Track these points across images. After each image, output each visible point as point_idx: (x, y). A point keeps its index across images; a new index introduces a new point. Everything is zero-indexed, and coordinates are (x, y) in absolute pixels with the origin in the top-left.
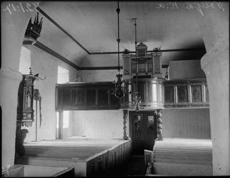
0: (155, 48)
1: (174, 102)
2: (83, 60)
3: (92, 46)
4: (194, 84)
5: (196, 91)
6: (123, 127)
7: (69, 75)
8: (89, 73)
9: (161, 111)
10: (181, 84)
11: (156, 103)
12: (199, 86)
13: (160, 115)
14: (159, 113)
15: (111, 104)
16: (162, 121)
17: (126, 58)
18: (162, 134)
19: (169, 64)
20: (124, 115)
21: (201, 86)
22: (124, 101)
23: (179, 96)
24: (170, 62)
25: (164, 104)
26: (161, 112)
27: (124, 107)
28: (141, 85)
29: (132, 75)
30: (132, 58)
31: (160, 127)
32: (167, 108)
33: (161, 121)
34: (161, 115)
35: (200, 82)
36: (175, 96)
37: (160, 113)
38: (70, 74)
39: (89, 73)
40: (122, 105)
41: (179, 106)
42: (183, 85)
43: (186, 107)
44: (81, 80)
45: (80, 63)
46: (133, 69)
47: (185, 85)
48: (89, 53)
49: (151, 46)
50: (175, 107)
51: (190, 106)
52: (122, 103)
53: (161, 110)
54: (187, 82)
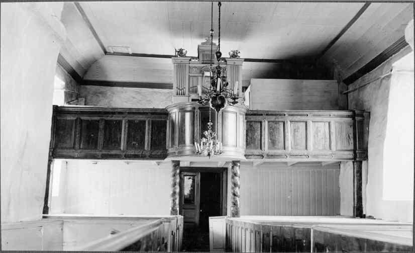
0: (232, 51)
1: (261, 149)
2: (90, 64)
3: (116, 43)
4: (273, 118)
5: (297, 131)
6: (172, 192)
7: (65, 92)
8: (101, 93)
9: (239, 164)
10: (274, 117)
11: (233, 149)
12: (258, 122)
13: (236, 171)
14: (235, 167)
15: (149, 149)
16: (240, 182)
17: (180, 67)
18: (239, 206)
19: (250, 84)
20: (173, 171)
21: (261, 123)
22: (177, 142)
23: (271, 139)
24: (253, 81)
25: (245, 151)
26: (239, 166)
27: (177, 154)
28: (206, 118)
29: (189, 96)
30: (191, 65)
31: (237, 193)
32: (250, 158)
33: (239, 183)
34: (239, 172)
35: (280, 115)
36: (264, 139)
37: (238, 168)
38: (68, 90)
39: (101, 93)
40: (170, 150)
41: (269, 156)
42: (277, 120)
43: (274, 158)
44: (86, 101)
45: (85, 72)
46: (191, 86)
47: (280, 120)
48: (106, 53)
49: (226, 47)
50: (264, 158)
51: (288, 157)
52: (172, 147)
53: (239, 162)
54: (285, 115)
